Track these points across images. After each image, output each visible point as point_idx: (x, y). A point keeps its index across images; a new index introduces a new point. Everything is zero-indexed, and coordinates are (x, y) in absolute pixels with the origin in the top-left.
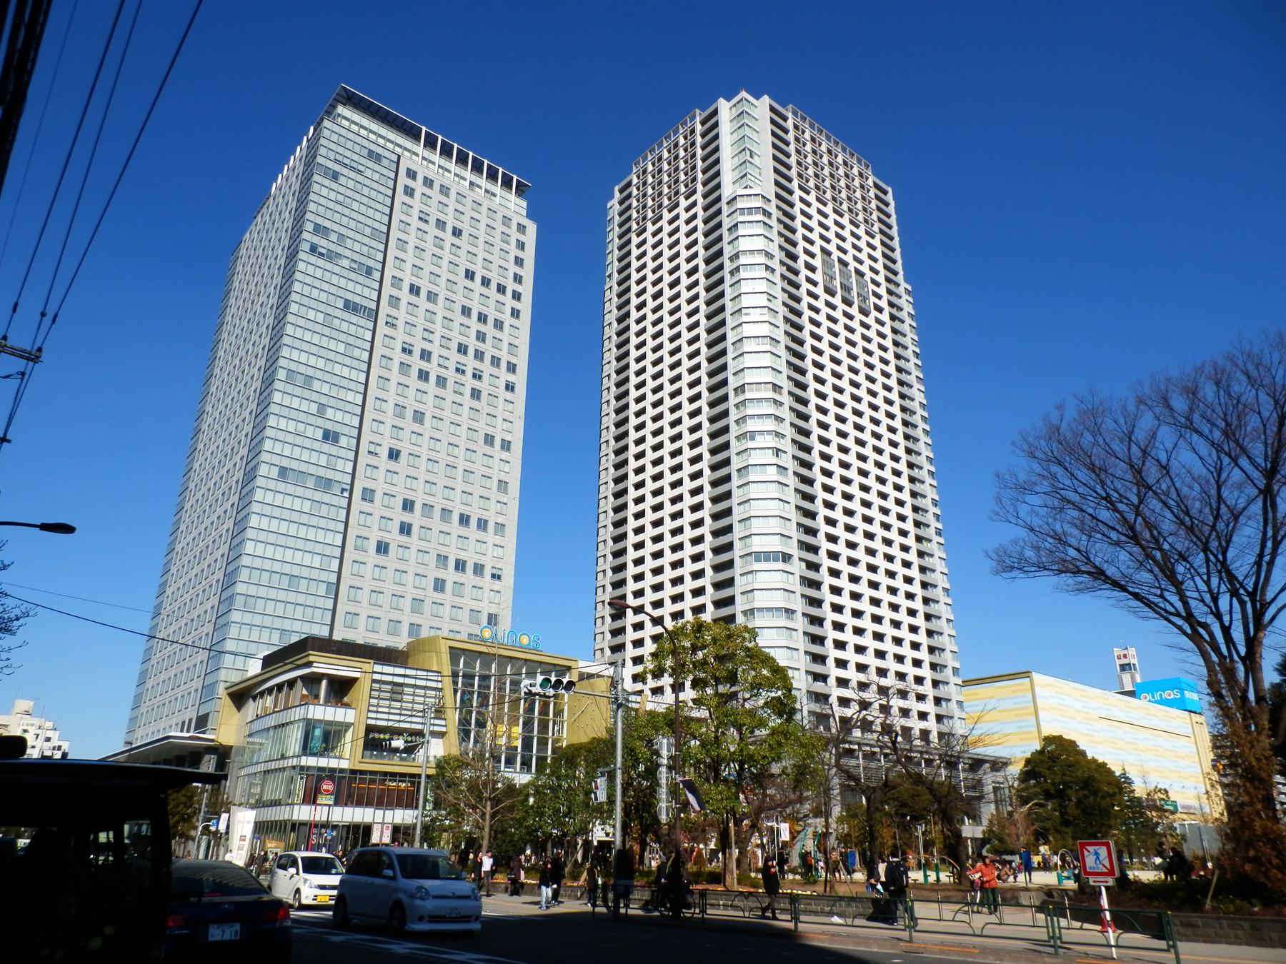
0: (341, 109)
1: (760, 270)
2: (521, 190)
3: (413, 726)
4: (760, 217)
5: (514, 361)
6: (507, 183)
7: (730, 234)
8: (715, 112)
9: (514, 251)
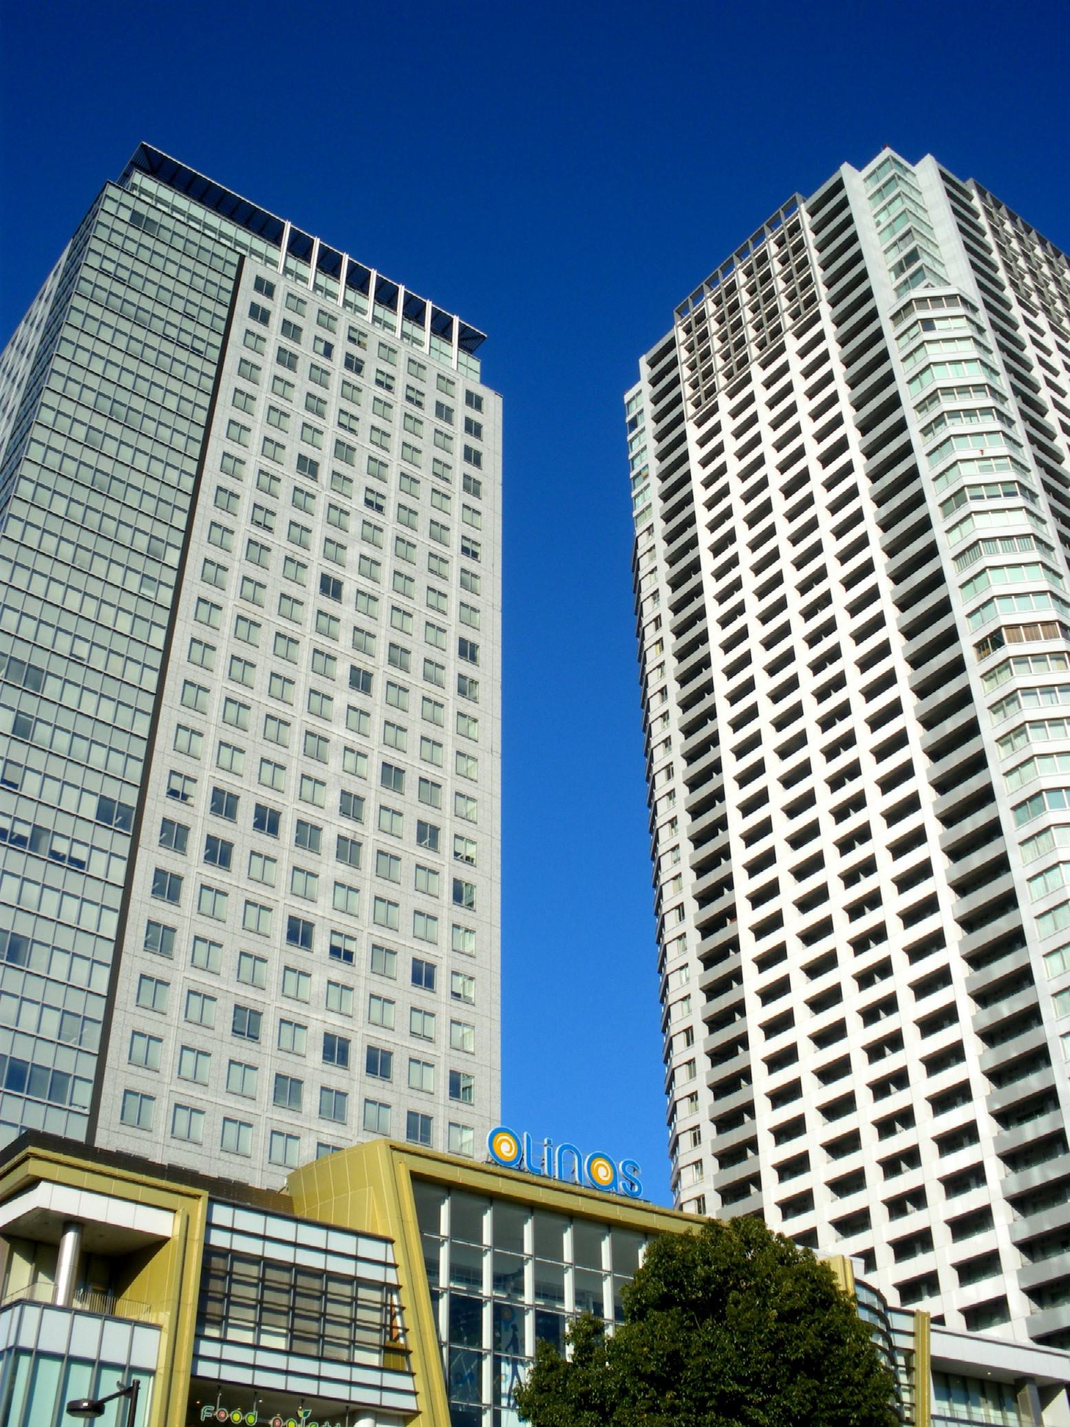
0: (137, 178)
1: (1024, 550)
2: (469, 343)
3: (329, 1390)
4: (961, 310)
5: (470, 636)
6: (441, 329)
7: (946, 515)
8: (839, 186)
9: (462, 437)
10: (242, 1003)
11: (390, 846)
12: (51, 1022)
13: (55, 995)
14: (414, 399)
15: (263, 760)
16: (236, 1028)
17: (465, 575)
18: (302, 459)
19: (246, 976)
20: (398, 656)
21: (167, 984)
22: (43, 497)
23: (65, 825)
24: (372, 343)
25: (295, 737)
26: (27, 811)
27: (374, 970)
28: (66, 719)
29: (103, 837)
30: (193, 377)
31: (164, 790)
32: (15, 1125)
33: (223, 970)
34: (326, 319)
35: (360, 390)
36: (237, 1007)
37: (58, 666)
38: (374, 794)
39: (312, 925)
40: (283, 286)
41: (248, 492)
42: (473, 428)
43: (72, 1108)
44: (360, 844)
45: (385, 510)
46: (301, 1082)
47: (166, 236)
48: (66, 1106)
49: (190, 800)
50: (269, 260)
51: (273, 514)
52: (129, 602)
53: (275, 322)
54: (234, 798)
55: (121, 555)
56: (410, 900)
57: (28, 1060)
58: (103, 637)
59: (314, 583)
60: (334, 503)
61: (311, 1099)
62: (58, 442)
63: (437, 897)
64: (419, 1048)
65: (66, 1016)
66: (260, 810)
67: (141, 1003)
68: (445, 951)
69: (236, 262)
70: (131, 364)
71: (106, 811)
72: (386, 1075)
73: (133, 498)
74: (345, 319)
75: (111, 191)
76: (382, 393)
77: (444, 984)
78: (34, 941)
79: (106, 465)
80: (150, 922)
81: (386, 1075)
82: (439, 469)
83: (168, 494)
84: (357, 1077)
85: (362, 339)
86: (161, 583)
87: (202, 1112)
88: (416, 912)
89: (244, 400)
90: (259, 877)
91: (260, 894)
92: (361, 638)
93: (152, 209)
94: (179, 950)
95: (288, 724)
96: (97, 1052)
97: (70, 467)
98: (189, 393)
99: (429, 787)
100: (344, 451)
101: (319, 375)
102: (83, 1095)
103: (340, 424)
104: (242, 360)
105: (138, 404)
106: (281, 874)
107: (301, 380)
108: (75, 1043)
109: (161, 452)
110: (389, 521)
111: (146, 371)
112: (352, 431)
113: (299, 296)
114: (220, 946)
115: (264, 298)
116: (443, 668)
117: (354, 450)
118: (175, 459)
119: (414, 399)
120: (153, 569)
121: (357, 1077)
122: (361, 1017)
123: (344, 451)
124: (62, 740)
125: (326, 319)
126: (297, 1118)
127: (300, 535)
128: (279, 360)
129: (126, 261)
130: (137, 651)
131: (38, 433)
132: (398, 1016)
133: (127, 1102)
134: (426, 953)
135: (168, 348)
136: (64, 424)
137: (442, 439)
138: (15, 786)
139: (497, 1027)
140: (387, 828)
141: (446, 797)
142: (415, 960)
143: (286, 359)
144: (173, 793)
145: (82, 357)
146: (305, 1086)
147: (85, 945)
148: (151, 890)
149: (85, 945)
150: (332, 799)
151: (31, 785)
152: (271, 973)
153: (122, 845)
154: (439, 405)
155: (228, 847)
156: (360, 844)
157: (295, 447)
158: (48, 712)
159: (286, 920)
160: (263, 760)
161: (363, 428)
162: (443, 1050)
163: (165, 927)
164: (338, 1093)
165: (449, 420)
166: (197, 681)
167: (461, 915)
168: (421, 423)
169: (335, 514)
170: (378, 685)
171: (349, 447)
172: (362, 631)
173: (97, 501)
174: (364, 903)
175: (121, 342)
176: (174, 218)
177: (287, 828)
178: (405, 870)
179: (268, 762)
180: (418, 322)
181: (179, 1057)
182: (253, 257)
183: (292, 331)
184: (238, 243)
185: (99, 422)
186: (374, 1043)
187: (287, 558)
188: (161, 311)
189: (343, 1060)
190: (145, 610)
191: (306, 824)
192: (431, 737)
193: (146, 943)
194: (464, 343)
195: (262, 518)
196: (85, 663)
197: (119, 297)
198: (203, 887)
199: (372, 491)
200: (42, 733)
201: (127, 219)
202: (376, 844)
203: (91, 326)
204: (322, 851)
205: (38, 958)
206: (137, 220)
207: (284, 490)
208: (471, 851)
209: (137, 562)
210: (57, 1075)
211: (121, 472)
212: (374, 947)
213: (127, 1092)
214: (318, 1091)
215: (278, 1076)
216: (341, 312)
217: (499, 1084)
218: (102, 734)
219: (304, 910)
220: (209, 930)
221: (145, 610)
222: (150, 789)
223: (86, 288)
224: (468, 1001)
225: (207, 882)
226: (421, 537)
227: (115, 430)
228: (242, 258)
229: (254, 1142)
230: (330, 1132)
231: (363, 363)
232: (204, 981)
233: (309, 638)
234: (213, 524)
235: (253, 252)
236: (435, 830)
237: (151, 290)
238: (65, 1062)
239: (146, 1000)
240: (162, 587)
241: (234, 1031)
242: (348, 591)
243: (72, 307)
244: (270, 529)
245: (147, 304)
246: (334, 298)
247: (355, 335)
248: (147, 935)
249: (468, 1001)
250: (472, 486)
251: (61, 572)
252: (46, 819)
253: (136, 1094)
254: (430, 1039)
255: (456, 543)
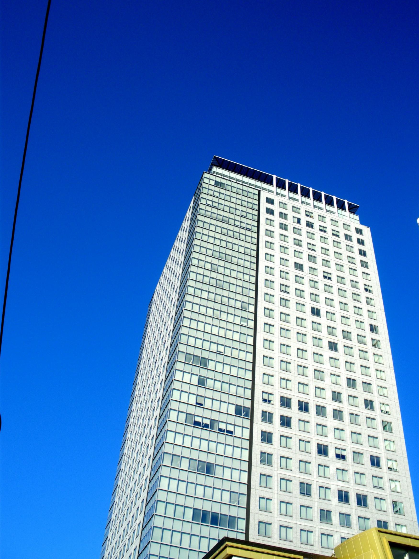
0: (215, 169)
2: (353, 209)
5: (374, 323)
6: (341, 206)
9: (357, 247)
10: (302, 481)
11: (355, 410)
12: (226, 497)
13: (227, 485)
14: (336, 234)
15: (299, 383)
16: (301, 492)
17: (367, 299)
18: (296, 264)
19: (303, 470)
20: (346, 335)
21: (271, 477)
22: (198, 292)
23: (223, 418)
24: (315, 215)
25: (310, 372)
26: (207, 414)
27: (355, 462)
28: (219, 377)
29: (239, 421)
30: (248, 239)
31: (261, 400)
32: (216, 539)
33: (293, 469)
34: (296, 209)
35: (314, 234)
36: (301, 483)
37: (213, 356)
38: (345, 391)
39: (327, 446)
40: (277, 199)
41: (277, 280)
42: (361, 242)
43: (238, 531)
44: (342, 412)
45: (332, 279)
46: (330, 512)
47: (229, 188)
48: (236, 530)
49: (272, 402)
50: (269, 191)
51: (289, 287)
52: (237, 328)
53: (277, 213)
54: (289, 399)
55: (231, 310)
56: (365, 432)
57: (219, 512)
58: (229, 343)
59: (309, 311)
60: (311, 279)
61: (335, 518)
62: (201, 271)
63: (376, 429)
64: (378, 492)
65: (232, 493)
66: (300, 403)
67: (261, 485)
68: (383, 451)
69: (257, 193)
70: (224, 238)
71: (239, 411)
72: (365, 505)
73: (233, 288)
74: (316, 212)
75: (206, 175)
76: (323, 234)
77: (384, 464)
78: (216, 465)
79: (220, 277)
80: (262, 453)
81: (365, 505)
82: (350, 260)
83: (246, 285)
84: (354, 507)
85: (311, 214)
86: (249, 319)
87: (291, 528)
88: (369, 436)
89: (269, 245)
90: (303, 430)
91: (305, 436)
92: (331, 330)
93: (222, 179)
94: (275, 463)
95: (306, 368)
96: (246, 507)
97: (206, 280)
98: (248, 245)
99: (367, 385)
100: (312, 258)
101: (297, 231)
102: (242, 525)
103: (309, 248)
104: (266, 230)
105: (229, 252)
106: (312, 427)
107: (290, 233)
108: (237, 504)
109: (241, 269)
110: (334, 282)
111: (230, 239)
112: (314, 250)
113: (284, 202)
114: (291, 459)
115: (271, 205)
116: (365, 337)
117: (315, 257)
118: (247, 271)
119: (336, 234)
120: (245, 314)
121: (354, 507)
122: (352, 481)
123: (312, 258)
124: (218, 385)
125: (296, 209)
126: (331, 527)
127: (300, 292)
128: (281, 228)
129: (216, 200)
130: (243, 347)
131: (192, 268)
132: (367, 480)
133: (260, 527)
134: (375, 452)
135: (237, 229)
136: (202, 264)
137: (349, 248)
138: (201, 405)
139: (409, 480)
140: (319, 395)
141: (374, 388)
142: (371, 456)
143: (283, 227)
144: (265, 400)
145: (205, 238)
146: (332, 513)
147: (236, 464)
148: (260, 439)
149: (236, 464)
150: (328, 395)
151: (208, 403)
152: (313, 467)
153: (247, 423)
154: (346, 235)
155: (289, 419)
156: (342, 412)
157: (292, 260)
158: (211, 375)
159: (316, 445)
160: (299, 383)
161: (318, 248)
162: (388, 492)
163: (268, 454)
164: (346, 515)
165: (351, 240)
166: (268, 355)
167: (387, 435)
168: (340, 243)
169: (312, 283)
170: (340, 347)
171: (313, 257)
172: (330, 327)
173: (219, 291)
174: (347, 435)
175: (219, 230)
176: (231, 181)
177: (312, 409)
178: (362, 419)
179: (301, 384)
180: (343, 209)
181: (279, 506)
182: (263, 190)
183: (283, 216)
184: (256, 186)
185: (215, 261)
186: (359, 492)
187: (297, 303)
188: (232, 216)
189: (347, 500)
190: (244, 330)
191: (319, 406)
192: (365, 365)
193: (261, 461)
194: (350, 210)
195: (284, 289)
196: (223, 354)
197: (204, 210)
198: (281, 436)
199: (325, 272)
200: (210, 383)
201: (213, 184)
202: (348, 410)
203: (207, 226)
204: (327, 416)
205: (218, 471)
206: (217, 184)
207: (291, 277)
208: (387, 409)
209: (238, 312)
210: (231, 518)
211: (227, 279)
212: (354, 452)
213: (260, 522)
214: (338, 514)
215: (321, 510)
216: (289, 201)
217: (414, 505)
218: (234, 381)
219: (323, 441)
220: (286, 453)
221: (244, 330)
222: (255, 400)
223: (202, 212)
224: (396, 471)
225: (283, 434)
226: (348, 287)
227: (222, 263)
228: (259, 192)
229: (315, 538)
230: (345, 532)
231: (313, 223)
232: (287, 474)
233: (310, 333)
234: (265, 294)
235: (263, 189)
236: (372, 402)
237: (227, 209)
238: (234, 512)
239: (263, 484)
240: (249, 321)
241: (300, 493)
242: (323, 312)
243: (198, 220)
244: (288, 293)
245: (226, 214)
246: (297, 201)
247: (308, 214)
248: (261, 457)
249: (396, 471)
250: (364, 264)
251: (209, 320)
252: (215, 416)
253: (264, 523)
254: (381, 488)
255: (362, 288)
